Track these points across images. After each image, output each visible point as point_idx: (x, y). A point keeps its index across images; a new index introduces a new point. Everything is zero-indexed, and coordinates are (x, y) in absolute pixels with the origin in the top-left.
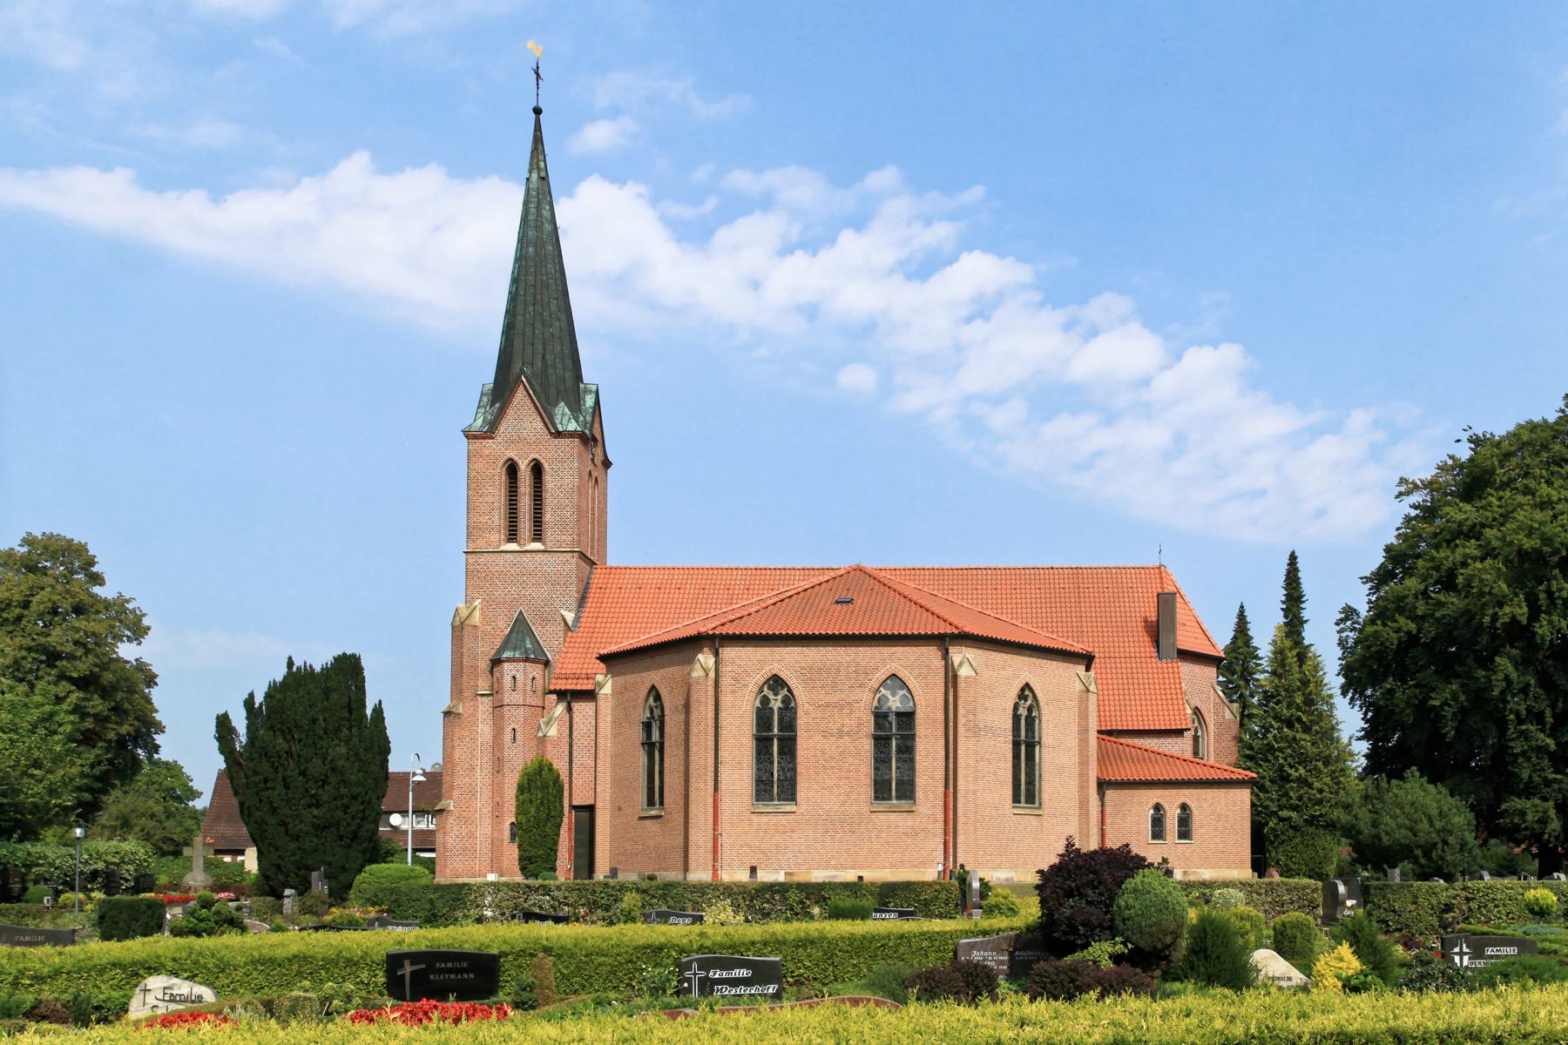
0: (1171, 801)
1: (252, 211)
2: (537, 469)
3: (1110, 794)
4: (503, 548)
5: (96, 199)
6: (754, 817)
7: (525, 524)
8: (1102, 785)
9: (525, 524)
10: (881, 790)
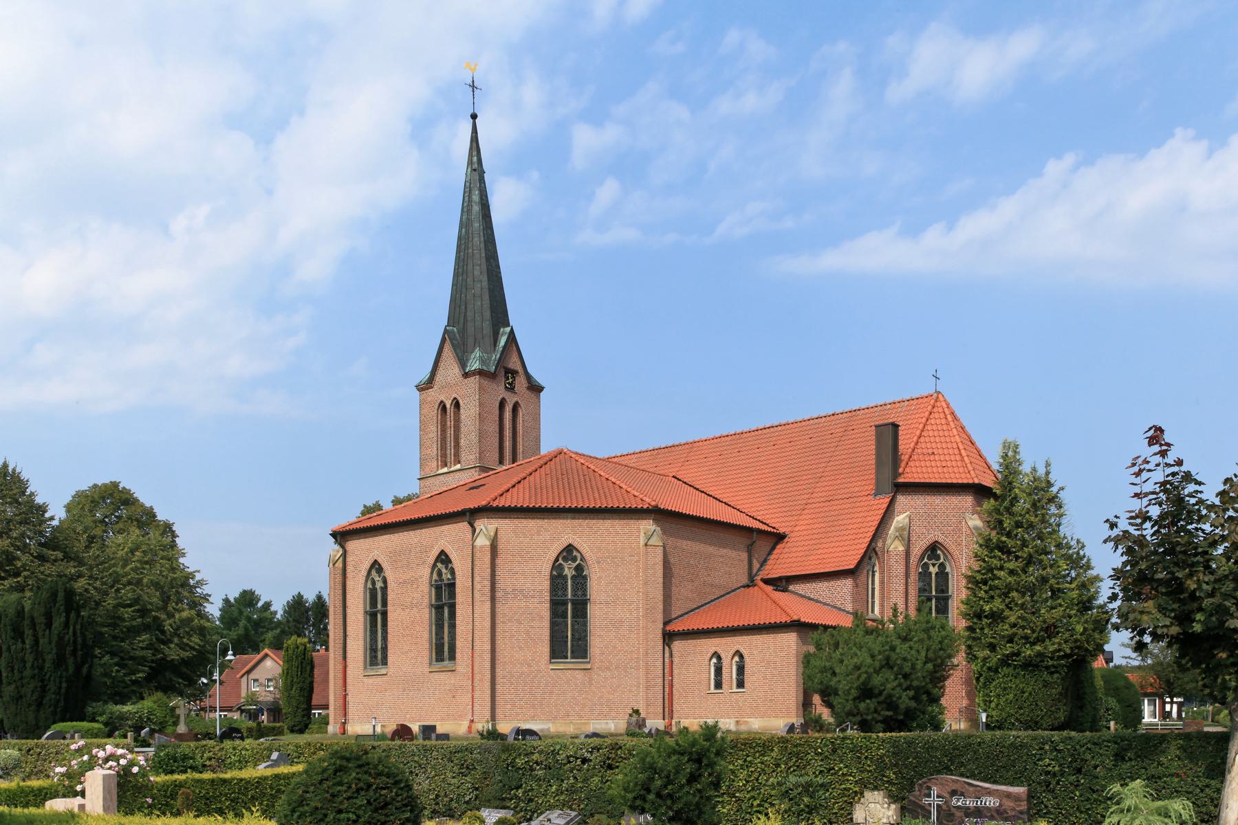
0: (727, 646)
1: (976, 225)
2: (457, 405)
3: (677, 645)
4: (441, 471)
5: (880, 253)
6: (365, 680)
7: (450, 451)
8: (669, 637)
9: (450, 451)
10: (557, 652)
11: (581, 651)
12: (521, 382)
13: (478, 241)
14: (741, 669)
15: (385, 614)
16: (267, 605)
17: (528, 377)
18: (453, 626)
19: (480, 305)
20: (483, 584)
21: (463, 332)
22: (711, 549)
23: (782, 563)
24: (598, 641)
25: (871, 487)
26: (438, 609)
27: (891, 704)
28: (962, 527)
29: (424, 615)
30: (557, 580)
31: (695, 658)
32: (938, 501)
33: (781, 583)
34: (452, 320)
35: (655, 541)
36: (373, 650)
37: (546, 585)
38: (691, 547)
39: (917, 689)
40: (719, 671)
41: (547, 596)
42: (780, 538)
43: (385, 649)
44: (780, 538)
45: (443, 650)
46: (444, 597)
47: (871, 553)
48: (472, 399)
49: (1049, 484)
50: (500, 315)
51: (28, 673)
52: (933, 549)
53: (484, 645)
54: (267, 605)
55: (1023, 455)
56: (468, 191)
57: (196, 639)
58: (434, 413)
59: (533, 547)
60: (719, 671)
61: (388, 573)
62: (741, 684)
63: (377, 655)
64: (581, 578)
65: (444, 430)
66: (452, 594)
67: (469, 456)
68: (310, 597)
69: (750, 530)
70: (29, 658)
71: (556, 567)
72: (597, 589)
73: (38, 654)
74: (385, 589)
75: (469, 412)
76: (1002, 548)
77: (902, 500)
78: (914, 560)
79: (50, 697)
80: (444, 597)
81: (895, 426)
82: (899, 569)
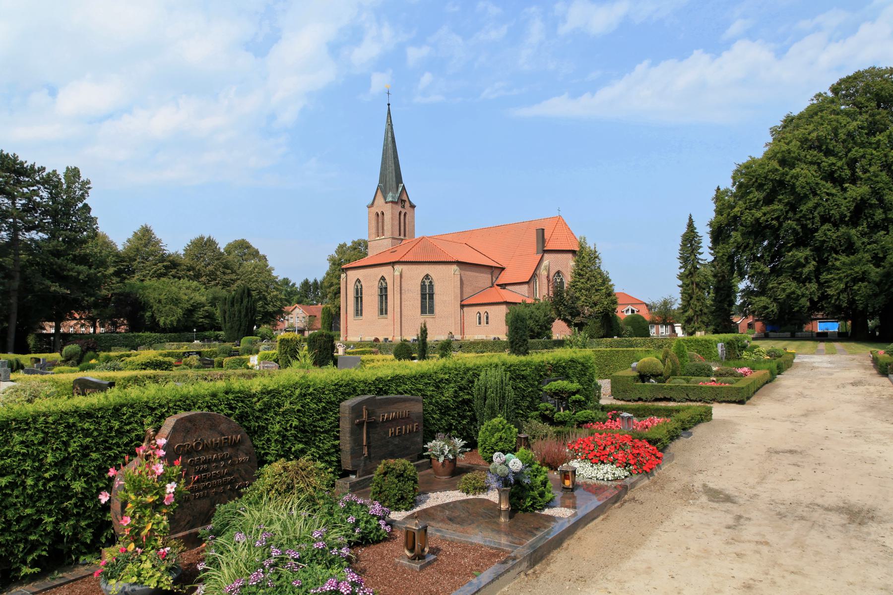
0: (482, 310)
2: (383, 214)
3: (465, 309)
7: (380, 231)
8: (462, 306)
9: (380, 231)
11: (432, 311)
12: (407, 205)
13: (390, 151)
14: (487, 318)
15: (361, 298)
16: (294, 285)
17: (410, 202)
18: (386, 302)
19: (392, 177)
20: (397, 288)
21: (385, 186)
22: (477, 274)
23: (504, 278)
24: (437, 308)
25: (535, 251)
26: (381, 296)
27: (532, 331)
28: (567, 265)
29: (376, 299)
30: (423, 286)
31: (471, 314)
32: (559, 256)
33: (503, 286)
34: (380, 182)
35: (458, 273)
36: (357, 310)
37: (419, 288)
38: (470, 274)
39: (541, 326)
40: (480, 318)
41: (419, 292)
42: (503, 269)
43: (361, 310)
44: (503, 269)
45: (383, 311)
46: (383, 292)
47: (534, 275)
48: (389, 212)
49: (596, 252)
50: (399, 179)
51: (236, 319)
52: (558, 272)
53: (398, 310)
54: (294, 285)
55: (587, 241)
56: (386, 133)
57: (279, 303)
58: (374, 216)
59: (414, 276)
60: (480, 318)
61: (362, 283)
62: (487, 323)
63: (359, 312)
64: (431, 285)
65: (378, 223)
66: (386, 291)
67: (388, 233)
68: (311, 281)
69: (491, 267)
70: (237, 314)
71: (423, 282)
72: (437, 289)
73: (240, 312)
74: (361, 289)
75: (388, 216)
76: (580, 275)
77: (546, 255)
78: (551, 277)
79: (242, 328)
80: (383, 292)
81: (543, 230)
82: (545, 281)
